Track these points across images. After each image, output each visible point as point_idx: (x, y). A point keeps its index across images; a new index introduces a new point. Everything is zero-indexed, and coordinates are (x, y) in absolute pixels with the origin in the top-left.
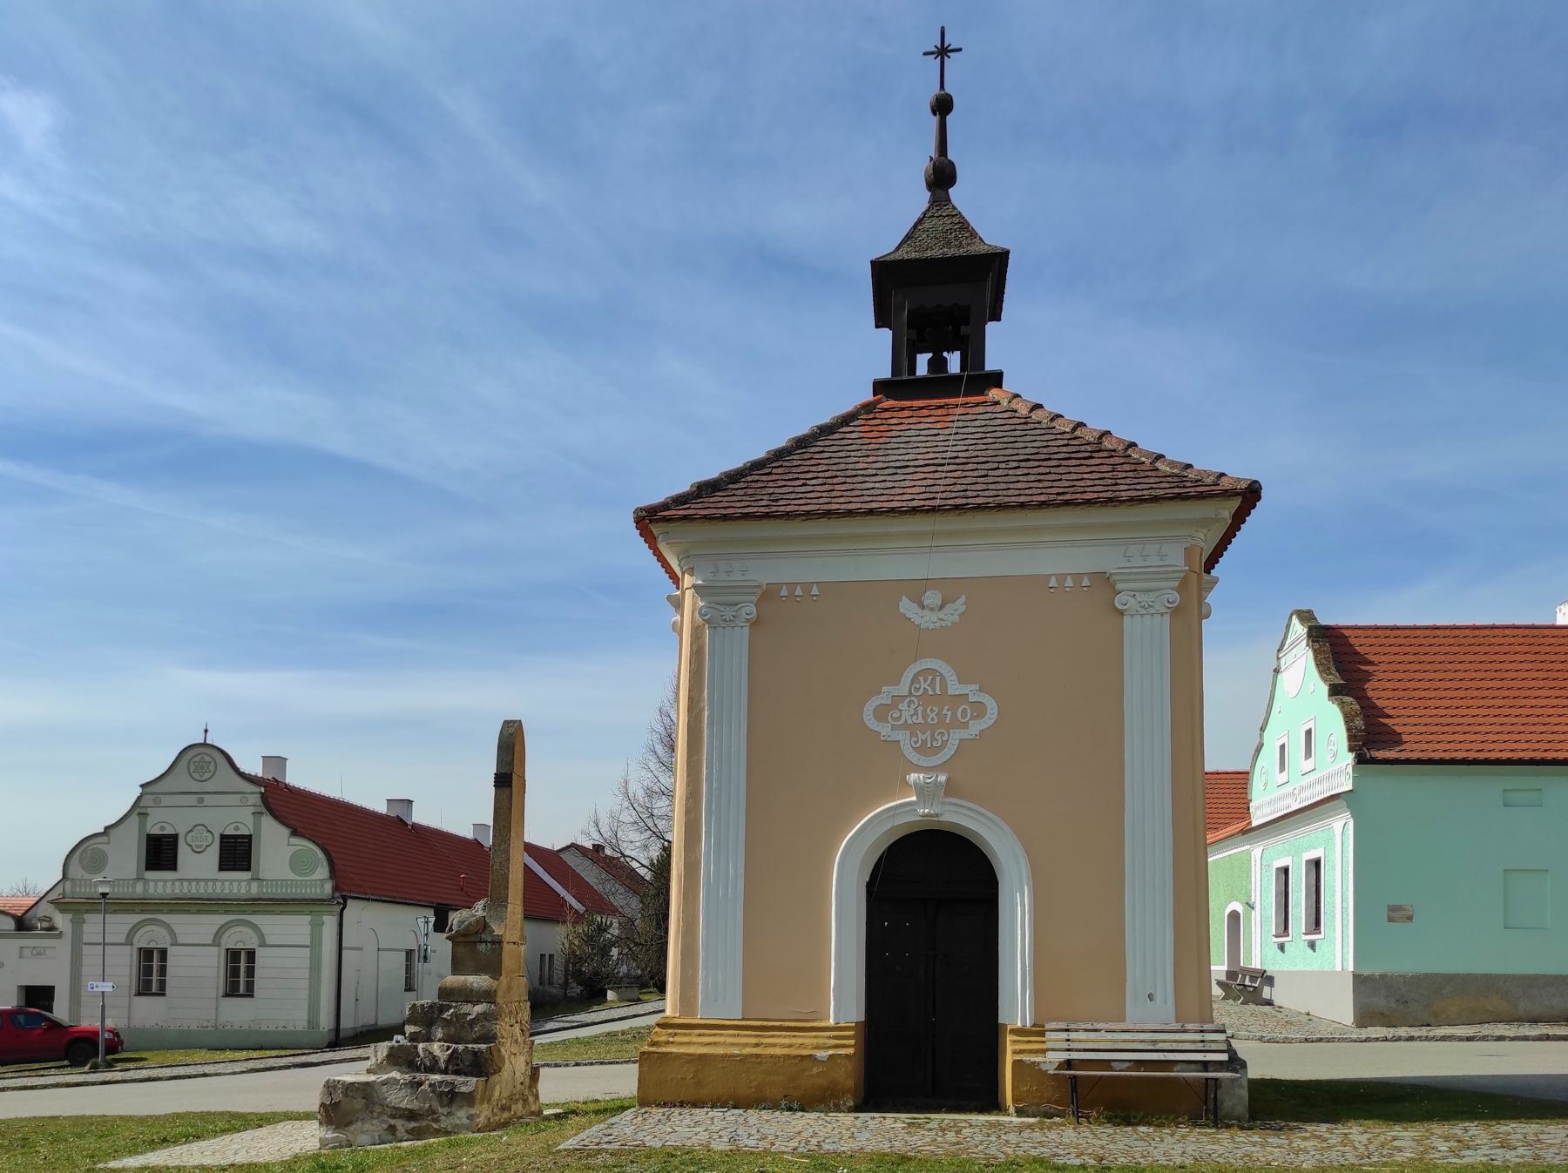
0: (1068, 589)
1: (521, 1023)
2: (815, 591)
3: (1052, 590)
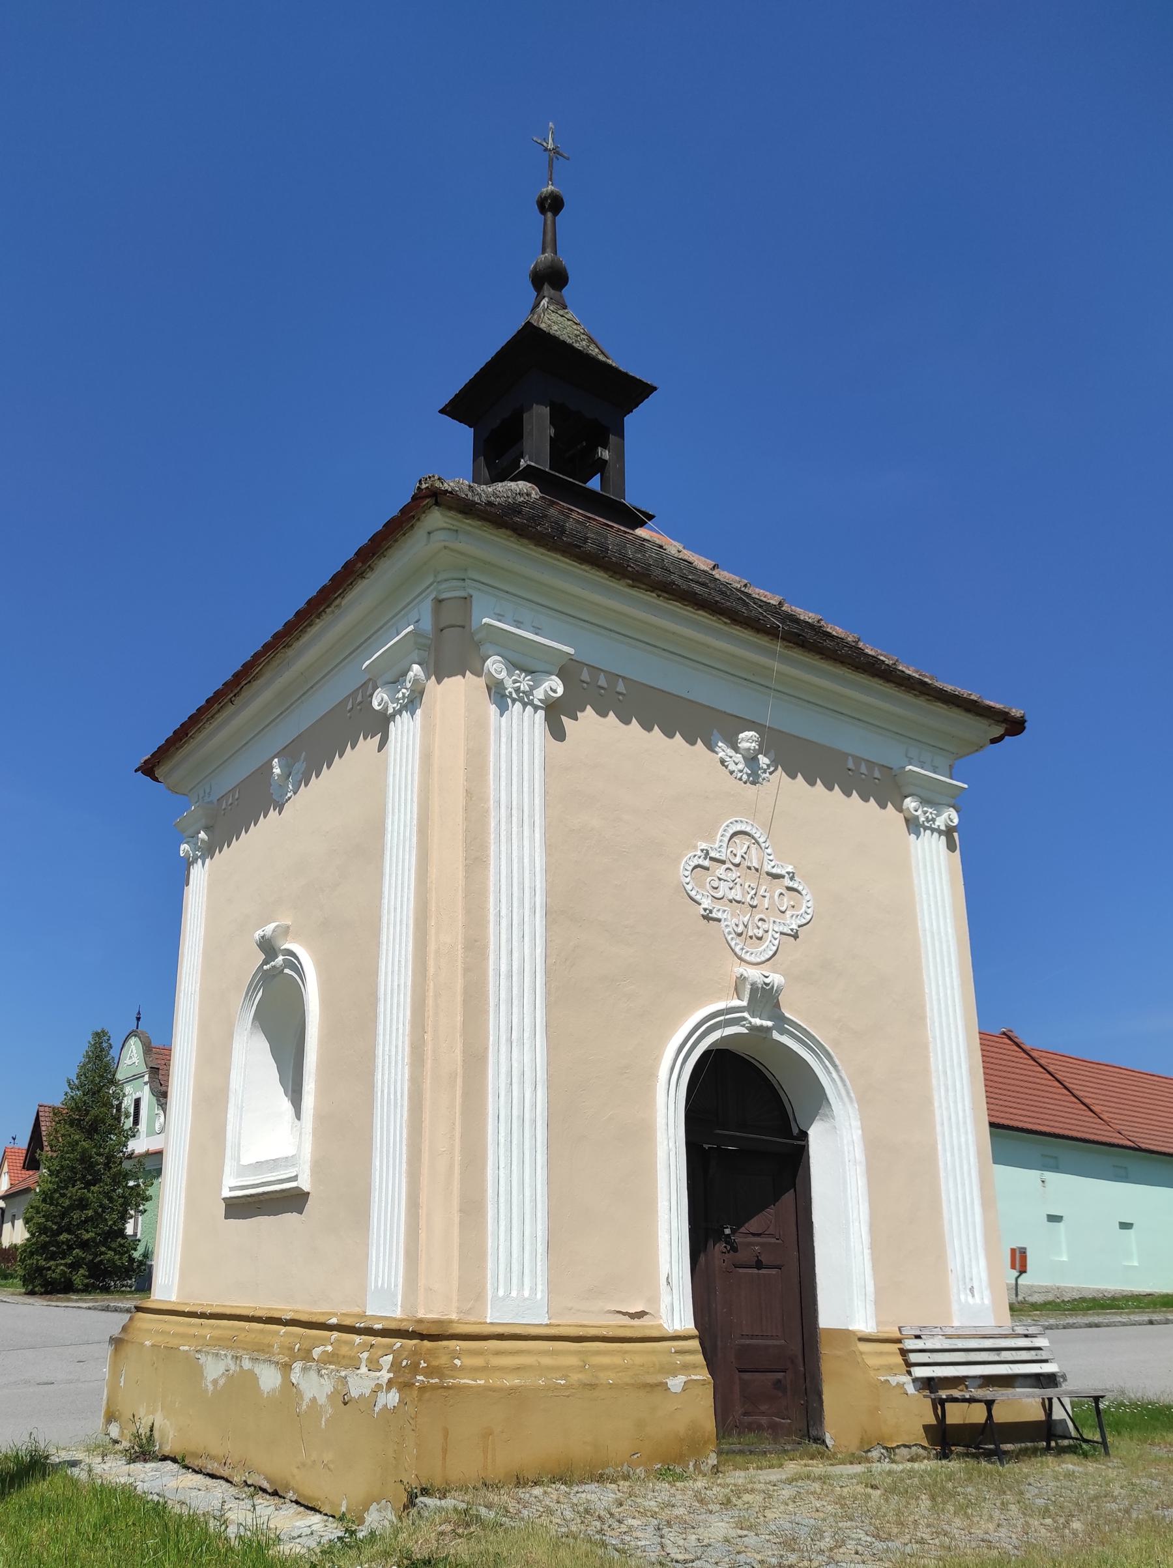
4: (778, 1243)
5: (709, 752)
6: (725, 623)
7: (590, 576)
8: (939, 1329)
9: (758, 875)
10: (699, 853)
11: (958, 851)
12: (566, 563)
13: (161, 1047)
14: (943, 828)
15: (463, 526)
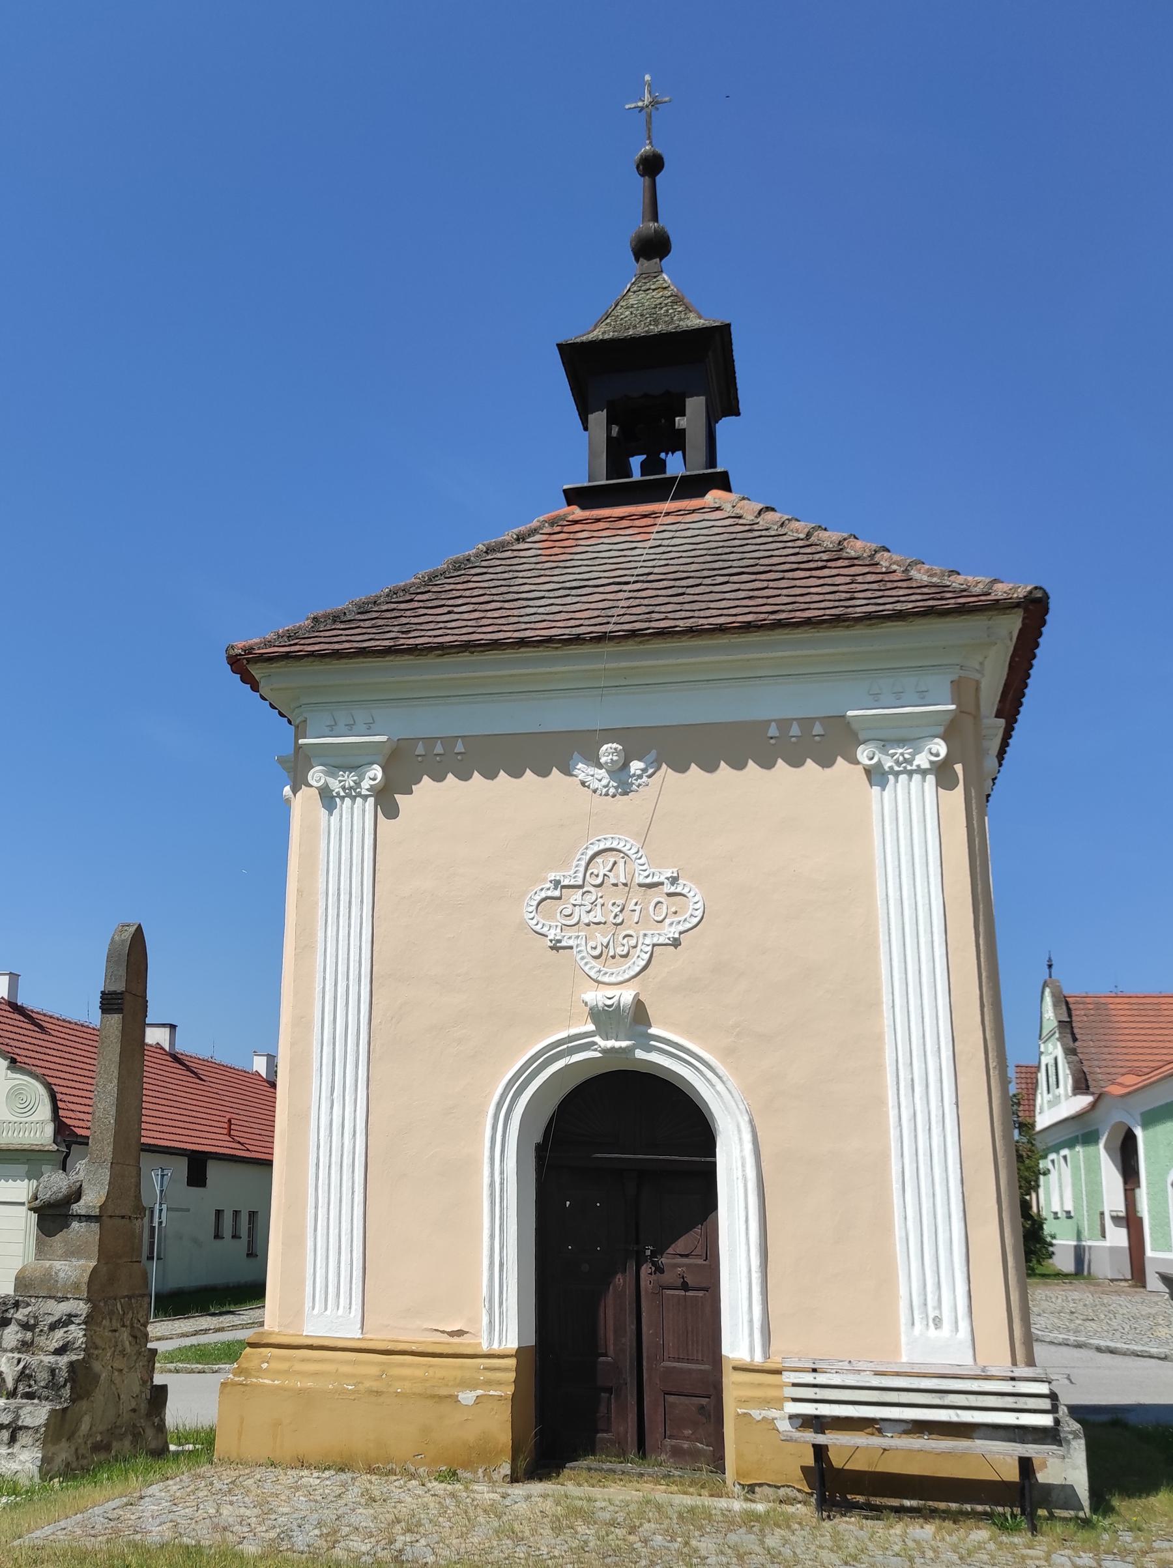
0: (793, 739)
1: (132, 1327)
2: (460, 748)
3: (772, 741)
4: (704, 1265)
5: (568, 777)
6: (557, 648)
7: (397, 663)
8: (846, 1363)
9: (627, 888)
10: (548, 885)
11: (960, 789)
12: (369, 662)
13: (1085, 995)
14: (925, 765)
15: (272, 671)
